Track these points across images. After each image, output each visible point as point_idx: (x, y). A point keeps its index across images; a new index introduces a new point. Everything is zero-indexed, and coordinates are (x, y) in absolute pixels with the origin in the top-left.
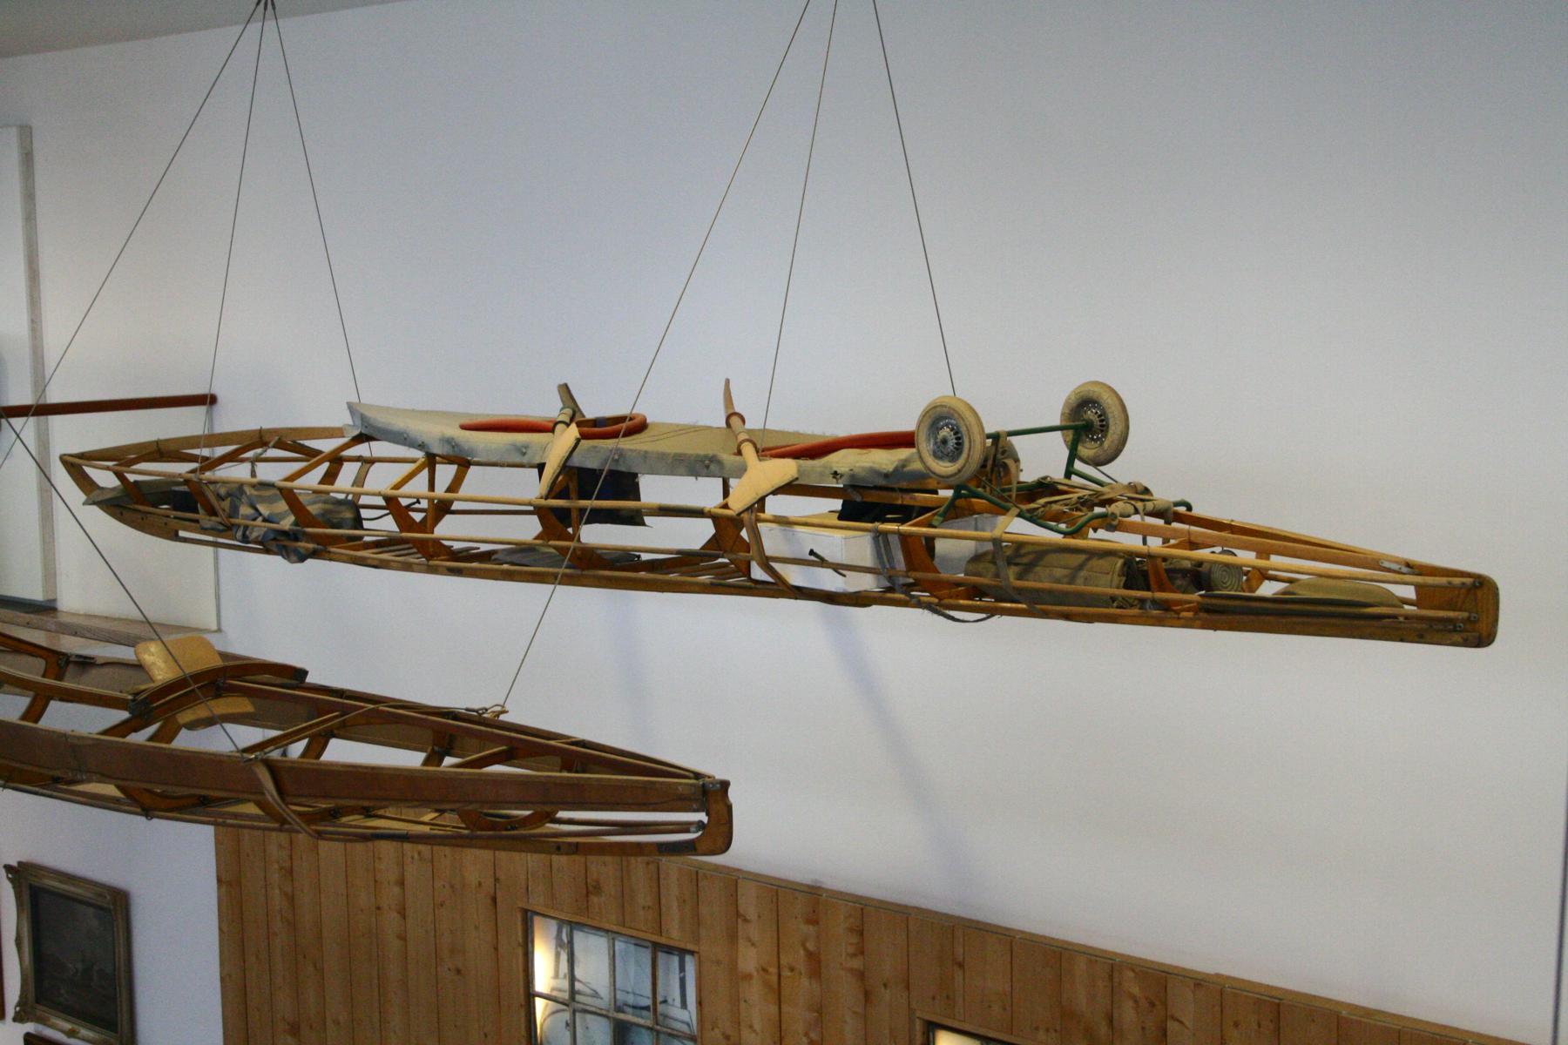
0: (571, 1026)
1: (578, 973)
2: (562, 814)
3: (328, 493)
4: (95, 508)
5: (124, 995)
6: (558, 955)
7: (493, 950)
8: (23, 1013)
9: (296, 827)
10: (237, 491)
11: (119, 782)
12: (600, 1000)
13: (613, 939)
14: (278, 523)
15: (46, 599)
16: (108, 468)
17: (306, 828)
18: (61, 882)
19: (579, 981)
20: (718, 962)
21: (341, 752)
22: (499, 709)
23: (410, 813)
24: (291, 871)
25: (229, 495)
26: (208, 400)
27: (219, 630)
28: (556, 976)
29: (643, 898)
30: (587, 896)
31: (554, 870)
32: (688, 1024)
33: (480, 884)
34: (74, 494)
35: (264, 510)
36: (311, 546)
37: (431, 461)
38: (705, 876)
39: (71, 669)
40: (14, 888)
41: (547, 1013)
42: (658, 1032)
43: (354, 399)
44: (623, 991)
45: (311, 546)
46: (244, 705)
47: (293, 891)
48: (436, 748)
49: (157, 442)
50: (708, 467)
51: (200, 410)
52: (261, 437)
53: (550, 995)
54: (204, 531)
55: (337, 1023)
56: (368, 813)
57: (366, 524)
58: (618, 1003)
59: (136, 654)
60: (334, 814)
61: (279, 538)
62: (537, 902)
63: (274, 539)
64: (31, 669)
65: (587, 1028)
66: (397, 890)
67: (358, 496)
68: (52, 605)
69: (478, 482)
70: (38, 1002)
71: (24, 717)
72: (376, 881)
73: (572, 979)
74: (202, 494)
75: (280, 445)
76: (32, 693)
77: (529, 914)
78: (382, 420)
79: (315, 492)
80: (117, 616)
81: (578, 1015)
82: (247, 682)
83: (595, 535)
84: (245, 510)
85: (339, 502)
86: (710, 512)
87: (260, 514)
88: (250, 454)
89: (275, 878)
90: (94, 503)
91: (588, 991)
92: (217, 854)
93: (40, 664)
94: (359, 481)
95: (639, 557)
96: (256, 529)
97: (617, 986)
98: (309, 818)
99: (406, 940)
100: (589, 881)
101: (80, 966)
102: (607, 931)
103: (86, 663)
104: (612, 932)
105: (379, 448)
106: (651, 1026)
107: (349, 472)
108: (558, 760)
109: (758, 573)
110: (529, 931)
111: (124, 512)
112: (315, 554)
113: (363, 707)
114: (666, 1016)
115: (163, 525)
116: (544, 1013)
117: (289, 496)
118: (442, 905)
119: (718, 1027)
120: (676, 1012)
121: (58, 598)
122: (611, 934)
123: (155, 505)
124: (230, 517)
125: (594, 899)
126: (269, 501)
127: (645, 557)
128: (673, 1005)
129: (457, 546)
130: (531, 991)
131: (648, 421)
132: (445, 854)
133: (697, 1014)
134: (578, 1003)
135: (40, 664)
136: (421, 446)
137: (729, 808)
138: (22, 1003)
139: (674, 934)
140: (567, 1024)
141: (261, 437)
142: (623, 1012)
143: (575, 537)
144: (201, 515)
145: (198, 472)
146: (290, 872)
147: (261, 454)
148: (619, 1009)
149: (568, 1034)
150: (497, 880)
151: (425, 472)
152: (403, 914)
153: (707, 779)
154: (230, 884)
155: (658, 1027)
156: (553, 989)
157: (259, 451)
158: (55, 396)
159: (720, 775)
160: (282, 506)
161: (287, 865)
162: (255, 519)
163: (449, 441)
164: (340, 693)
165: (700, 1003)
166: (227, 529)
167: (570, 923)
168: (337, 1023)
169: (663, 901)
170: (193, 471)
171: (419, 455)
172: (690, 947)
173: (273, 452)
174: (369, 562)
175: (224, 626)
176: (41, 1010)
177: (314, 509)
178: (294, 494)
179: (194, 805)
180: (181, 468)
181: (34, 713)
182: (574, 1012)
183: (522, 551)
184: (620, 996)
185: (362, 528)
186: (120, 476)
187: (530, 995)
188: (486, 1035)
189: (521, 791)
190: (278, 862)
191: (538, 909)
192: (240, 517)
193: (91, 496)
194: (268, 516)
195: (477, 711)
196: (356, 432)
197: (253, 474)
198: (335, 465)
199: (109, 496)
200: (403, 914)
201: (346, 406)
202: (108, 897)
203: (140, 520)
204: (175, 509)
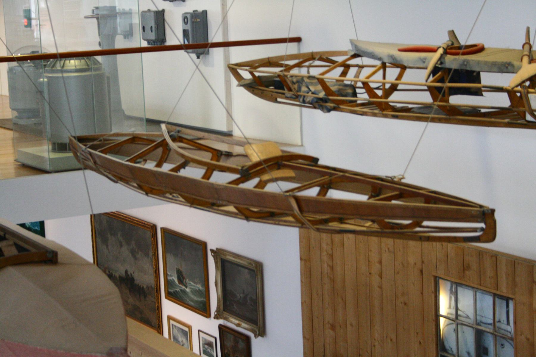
0: (456, 331)
1: (459, 306)
2: (425, 223)
3: (343, 81)
4: (242, 88)
5: (261, 309)
6: (450, 298)
7: (421, 294)
8: (218, 315)
9: (308, 226)
10: (300, 80)
11: (236, 205)
12: (469, 320)
13: (476, 292)
14: (318, 95)
15: (228, 130)
16: (246, 70)
17: (312, 227)
18: (234, 257)
19: (460, 310)
20: (524, 304)
21: (335, 194)
22: (401, 177)
23: (362, 222)
24: (332, 255)
25: (298, 82)
26: (298, 40)
27: (302, 145)
28: (450, 308)
29: (490, 273)
30: (464, 271)
31: (449, 259)
32: (510, 332)
33: (415, 264)
34: (234, 82)
35: (312, 88)
36: (332, 105)
37: (384, 66)
38: (519, 263)
39: (223, 157)
40: (214, 259)
41: (446, 324)
42: (496, 336)
43: (354, 37)
44: (480, 316)
45: (332, 105)
46: (290, 173)
47: (333, 265)
48: (373, 194)
49: (268, 58)
50: (507, 68)
51: (295, 44)
52: (312, 55)
53: (447, 316)
54: (287, 98)
55: (352, 325)
56: (341, 221)
57: (358, 95)
58: (478, 321)
59: (245, 150)
60: (325, 222)
61: (319, 101)
62: (441, 273)
63: (317, 102)
64: (206, 157)
65: (463, 332)
66: (378, 265)
67: (356, 82)
68: (230, 133)
69: (410, 76)
70: (224, 310)
71: (203, 177)
72: (369, 261)
73: (457, 309)
74: (286, 81)
75: (321, 59)
76: (206, 168)
77: (437, 278)
78: (364, 47)
79: (337, 81)
80: (258, 138)
81: (459, 326)
82: (294, 163)
83: (456, 100)
84: (304, 89)
85: (346, 85)
86: (506, 89)
87: (310, 91)
88: (307, 64)
89: (325, 258)
90: (241, 86)
91: (464, 315)
92: (300, 248)
93: (209, 155)
94: (357, 75)
95: (480, 111)
96: (309, 97)
97: (477, 313)
98: (315, 222)
99: (382, 289)
100: (465, 264)
101: (242, 295)
102: (473, 288)
103: (229, 155)
104: (475, 288)
105: (365, 61)
106: (492, 332)
107: (352, 72)
108: (423, 199)
109: (529, 118)
110: (437, 287)
111: (254, 90)
112: (335, 109)
113: (337, 174)
114: (500, 328)
115: (271, 96)
116: (444, 324)
117: (322, 82)
118: (398, 273)
119: (523, 334)
120: (504, 326)
121: (233, 131)
122: (475, 289)
123: (267, 87)
124: (297, 91)
125: (467, 272)
126: (315, 84)
127: (483, 110)
128: (503, 323)
129: (399, 105)
130: (438, 314)
131: (485, 47)
132: (374, 240)
133: (514, 326)
134: (460, 320)
135: (209, 155)
136: (380, 59)
137: (495, 222)
138: (218, 311)
139: (504, 290)
140: (454, 330)
141: (312, 55)
142: (480, 325)
143: (447, 101)
144: (286, 91)
145: (283, 71)
146: (331, 256)
147: (312, 63)
148: (478, 324)
149: (454, 335)
150: (423, 262)
151: (381, 71)
152: (381, 276)
153: (485, 209)
154: (305, 260)
155: (496, 333)
156: (448, 314)
157: (311, 62)
158: (232, 38)
159: (491, 207)
160: (319, 87)
161: (330, 252)
162: (308, 93)
163: (391, 57)
164: (335, 169)
165: (515, 323)
166: (296, 97)
167: (456, 283)
168: (352, 325)
169: (499, 274)
170: (281, 71)
171: (378, 63)
172: (510, 296)
173: (317, 63)
174: (358, 112)
175: (304, 144)
176: (226, 314)
177: (334, 89)
178: (324, 81)
179: (268, 216)
180: (277, 70)
181: (207, 176)
182: (457, 325)
183: (426, 107)
184: (478, 318)
185: (356, 97)
186: (252, 73)
187: (437, 316)
188: (417, 333)
189: (404, 213)
190: (326, 251)
191: (441, 276)
192: (302, 92)
193: (240, 82)
194: (315, 91)
195: (391, 177)
196: (353, 53)
197: (308, 72)
198: (346, 68)
199: (248, 82)
200: (381, 276)
201: (349, 41)
202: (254, 265)
203: (260, 93)
204: (276, 88)
